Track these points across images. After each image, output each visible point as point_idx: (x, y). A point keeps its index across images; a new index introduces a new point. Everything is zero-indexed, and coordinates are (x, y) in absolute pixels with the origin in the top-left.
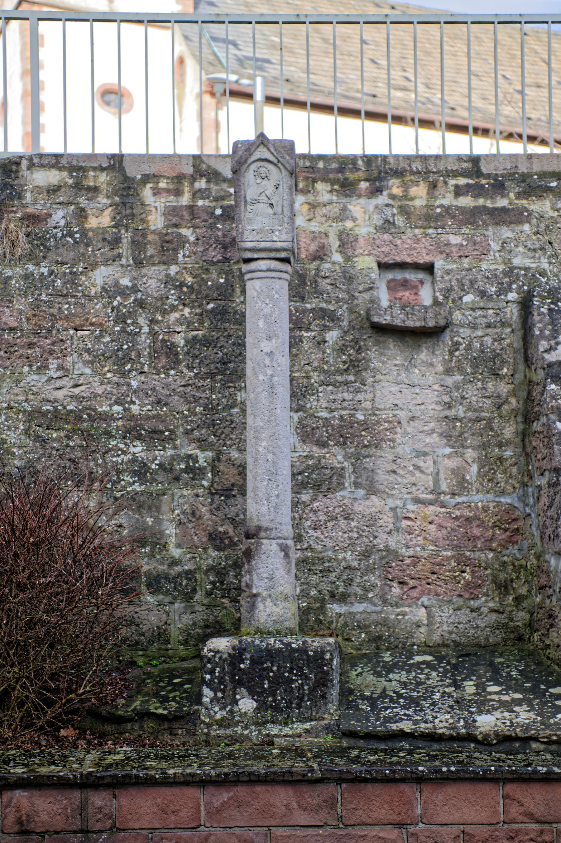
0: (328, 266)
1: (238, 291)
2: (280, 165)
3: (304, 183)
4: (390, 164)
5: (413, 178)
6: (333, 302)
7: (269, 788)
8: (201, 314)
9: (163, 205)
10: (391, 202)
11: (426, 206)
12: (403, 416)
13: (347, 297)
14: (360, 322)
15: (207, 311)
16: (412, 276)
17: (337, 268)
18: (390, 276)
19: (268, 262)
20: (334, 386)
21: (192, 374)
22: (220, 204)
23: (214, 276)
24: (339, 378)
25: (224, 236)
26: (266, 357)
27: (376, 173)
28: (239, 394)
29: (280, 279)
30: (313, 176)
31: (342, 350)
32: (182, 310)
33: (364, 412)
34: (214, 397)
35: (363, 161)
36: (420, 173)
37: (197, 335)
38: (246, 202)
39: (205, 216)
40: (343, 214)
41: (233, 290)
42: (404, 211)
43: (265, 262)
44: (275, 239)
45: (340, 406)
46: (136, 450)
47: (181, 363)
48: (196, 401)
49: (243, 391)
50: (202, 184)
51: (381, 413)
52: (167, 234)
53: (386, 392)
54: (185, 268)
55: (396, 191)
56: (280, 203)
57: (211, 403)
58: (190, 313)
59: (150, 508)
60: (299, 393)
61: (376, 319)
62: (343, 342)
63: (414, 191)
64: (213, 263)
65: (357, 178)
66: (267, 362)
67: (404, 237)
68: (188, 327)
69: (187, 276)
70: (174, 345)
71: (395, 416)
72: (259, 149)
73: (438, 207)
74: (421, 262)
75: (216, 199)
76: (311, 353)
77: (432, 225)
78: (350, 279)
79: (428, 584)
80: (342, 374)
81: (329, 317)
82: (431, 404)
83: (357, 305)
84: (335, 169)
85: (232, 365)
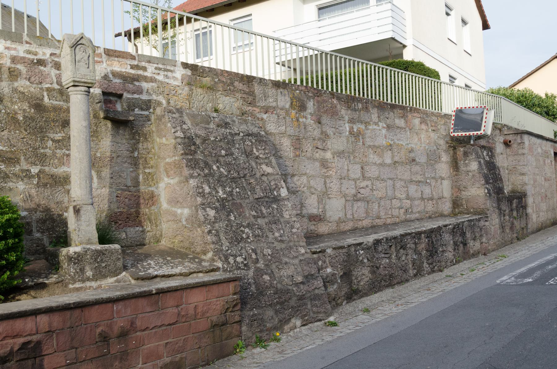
7: (137, 299)
18: (106, 97)
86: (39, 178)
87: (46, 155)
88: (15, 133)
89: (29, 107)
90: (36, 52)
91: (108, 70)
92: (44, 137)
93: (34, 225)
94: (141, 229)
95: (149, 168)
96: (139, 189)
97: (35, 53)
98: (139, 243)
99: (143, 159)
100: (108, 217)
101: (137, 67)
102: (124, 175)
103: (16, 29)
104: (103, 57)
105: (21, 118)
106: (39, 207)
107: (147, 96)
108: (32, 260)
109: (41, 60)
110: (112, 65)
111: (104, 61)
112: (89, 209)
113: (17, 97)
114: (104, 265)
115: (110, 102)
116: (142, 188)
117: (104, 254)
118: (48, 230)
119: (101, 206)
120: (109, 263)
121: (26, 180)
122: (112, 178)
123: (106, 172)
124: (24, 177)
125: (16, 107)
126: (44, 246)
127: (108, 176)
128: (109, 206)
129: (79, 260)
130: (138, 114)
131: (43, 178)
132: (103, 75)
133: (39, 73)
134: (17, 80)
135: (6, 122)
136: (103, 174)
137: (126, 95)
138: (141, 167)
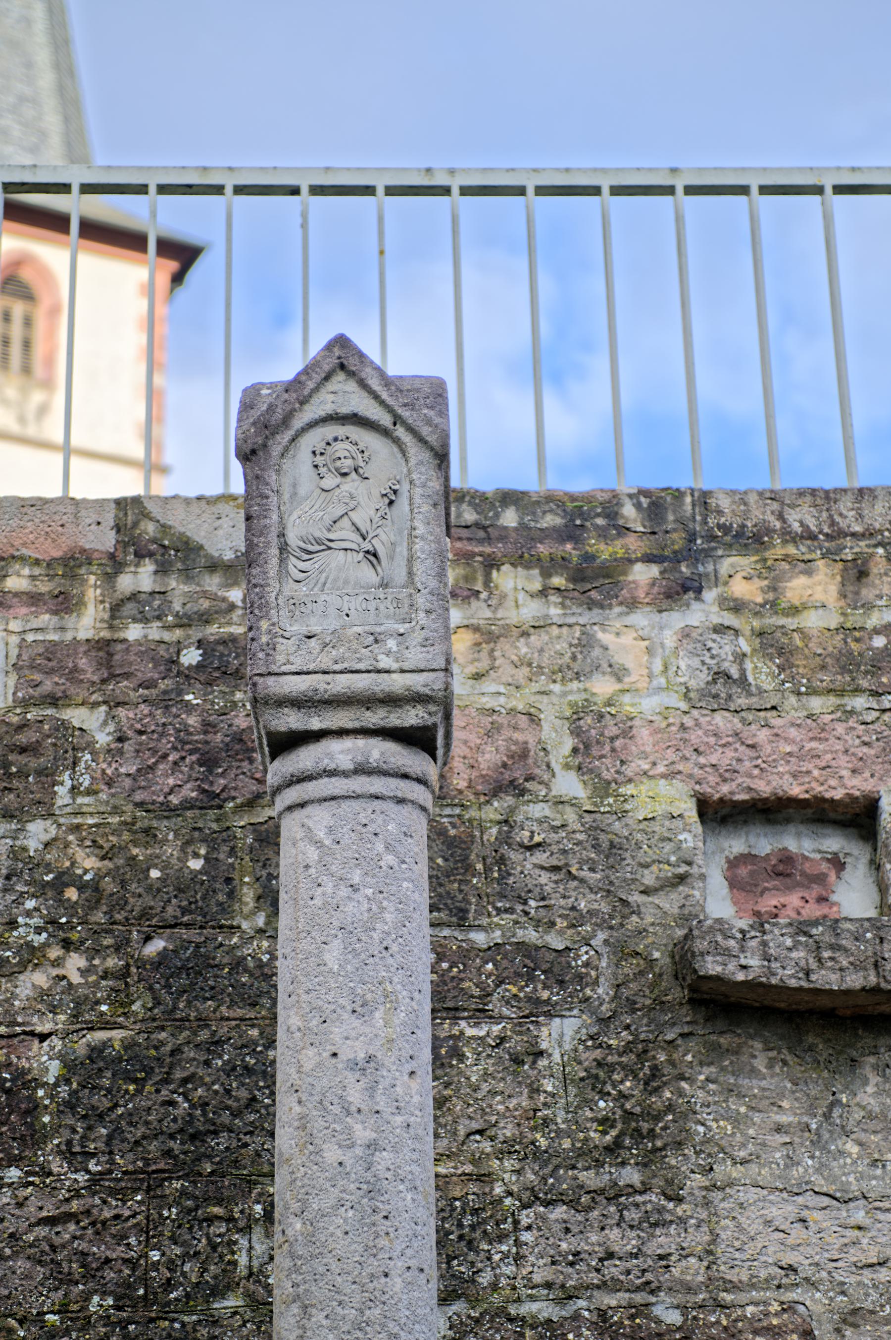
0: (538, 810)
1: (248, 895)
2: (400, 432)
3: (461, 571)
4: (720, 513)
5: (791, 550)
6: (561, 923)
8: (124, 974)
9: (14, 640)
10: (729, 619)
11: (841, 628)
12: (817, 1309)
13: (605, 908)
14: (653, 986)
15: (141, 963)
16: (806, 845)
17: (570, 816)
18: (736, 844)
19: (361, 742)
20: (573, 1204)
21: (82, 1177)
22: (196, 634)
23: (171, 851)
24: (589, 1178)
25: (208, 727)
26: (351, 1077)
27: (678, 540)
28: (244, 1242)
29: (401, 801)
30: (488, 550)
31: (595, 1081)
32: (57, 963)
33: (680, 1298)
34: (155, 1256)
35: (638, 506)
36: (813, 537)
37: (106, 1044)
38: (284, 548)
39: (148, 671)
40: (582, 661)
41: (231, 894)
42: (775, 646)
43: (348, 743)
44: (385, 662)
45: (594, 1278)
47: (45, 1138)
48: (89, 1275)
49: (258, 1232)
50: (141, 578)
51: (743, 1297)
52: (22, 727)
53: (751, 1222)
54: (77, 828)
55: (740, 588)
56: (402, 550)
57: (145, 1281)
58: (83, 972)
61: (712, 966)
62: (598, 1054)
63: (797, 588)
64: (169, 811)
65: (621, 553)
66: (355, 1096)
67: (777, 722)
68: (75, 1016)
69: (80, 854)
70: (25, 1080)
71: (788, 1308)
72: (331, 386)
73: (876, 631)
74: (838, 794)
75: (184, 622)
76: (493, 1093)
77: (864, 683)
78: (614, 851)
80: (599, 1164)
81: (548, 974)
83: (641, 932)
84: (554, 529)
85: (222, 1142)
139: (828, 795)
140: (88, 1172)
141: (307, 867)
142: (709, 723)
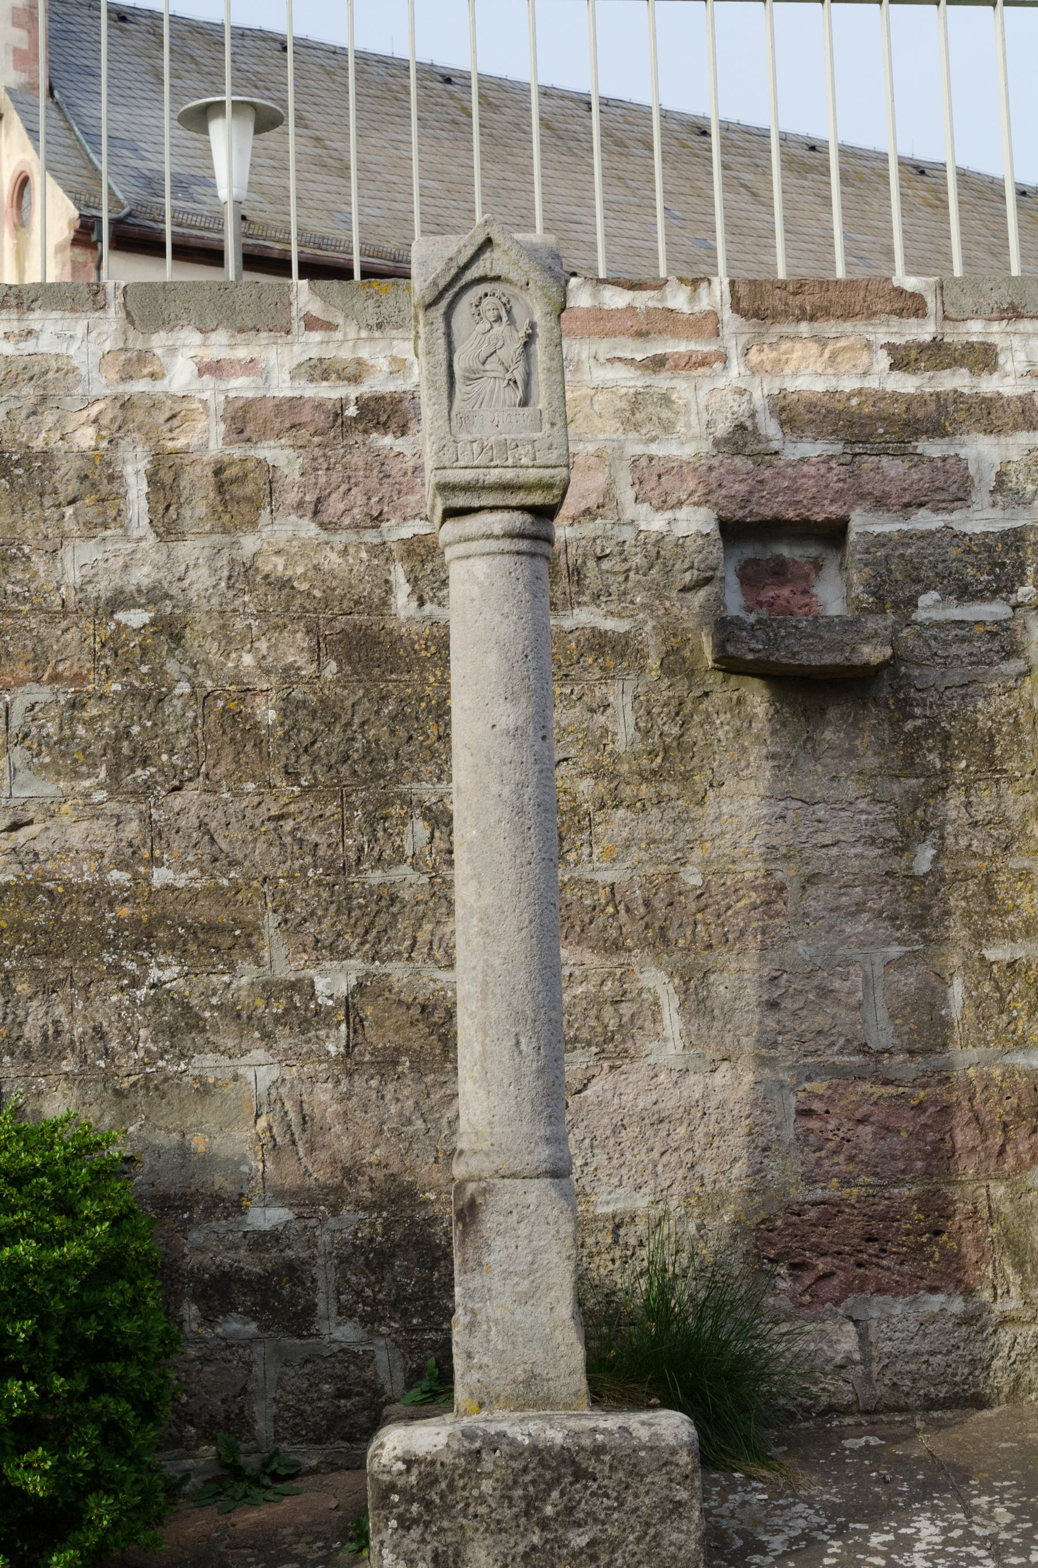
18: (749, 552)
46: (167, 974)
59: (109, 464)
60: (555, 827)
79: (860, 1265)
82: (853, 845)
86: (355, 1021)
87: (393, 899)
88: (238, 794)
89: (316, 654)
90: (359, 362)
91: (757, 395)
92: (388, 803)
93: (325, 1276)
94: (957, 1305)
95: (1010, 935)
96: (949, 1066)
97: (351, 371)
98: (943, 1392)
99: (972, 886)
100: (746, 1231)
101: (935, 354)
102: (848, 985)
103: (967, 262)
104: (726, 331)
105: (272, 715)
106: (353, 1181)
107: (996, 513)
108: (313, 1471)
109: (379, 399)
110: (777, 367)
111: (734, 355)
112: (532, 1199)
113: (252, 609)
114: (579, 1540)
115: (780, 571)
116: (967, 1058)
117: (580, 1474)
118: (400, 1304)
119: (707, 1169)
120: (613, 1531)
121: (284, 1039)
122: (773, 1005)
123: (738, 978)
124: (277, 1019)
125: (248, 660)
126: (378, 1392)
127: (751, 994)
128: (757, 1171)
129: (428, 1505)
130: (939, 625)
131: (379, 1023)
132: (722, 429)
133: (368, 467)
134: (254, 523)
135: (194, 743)
136: (721, 986)
137: (863, 523)
138: (957, 930)
139: (813, 518)
140: (300, 785)
141: (473, 600)
142: (730, 464)
